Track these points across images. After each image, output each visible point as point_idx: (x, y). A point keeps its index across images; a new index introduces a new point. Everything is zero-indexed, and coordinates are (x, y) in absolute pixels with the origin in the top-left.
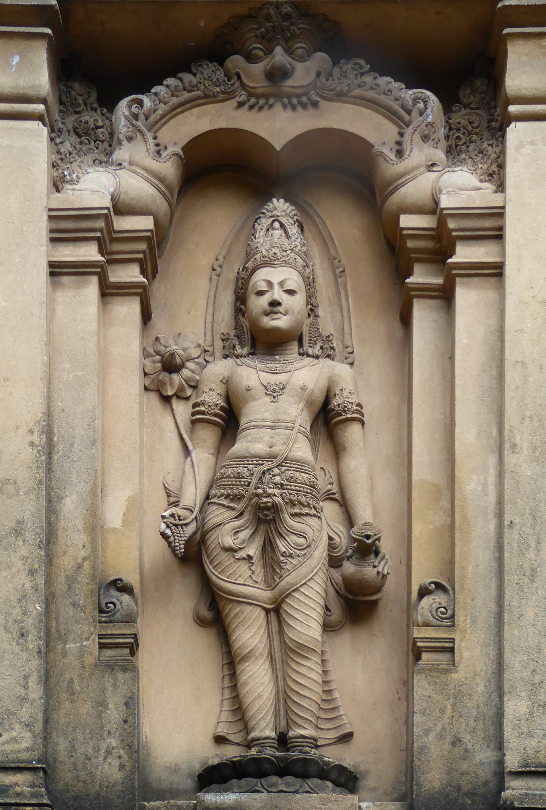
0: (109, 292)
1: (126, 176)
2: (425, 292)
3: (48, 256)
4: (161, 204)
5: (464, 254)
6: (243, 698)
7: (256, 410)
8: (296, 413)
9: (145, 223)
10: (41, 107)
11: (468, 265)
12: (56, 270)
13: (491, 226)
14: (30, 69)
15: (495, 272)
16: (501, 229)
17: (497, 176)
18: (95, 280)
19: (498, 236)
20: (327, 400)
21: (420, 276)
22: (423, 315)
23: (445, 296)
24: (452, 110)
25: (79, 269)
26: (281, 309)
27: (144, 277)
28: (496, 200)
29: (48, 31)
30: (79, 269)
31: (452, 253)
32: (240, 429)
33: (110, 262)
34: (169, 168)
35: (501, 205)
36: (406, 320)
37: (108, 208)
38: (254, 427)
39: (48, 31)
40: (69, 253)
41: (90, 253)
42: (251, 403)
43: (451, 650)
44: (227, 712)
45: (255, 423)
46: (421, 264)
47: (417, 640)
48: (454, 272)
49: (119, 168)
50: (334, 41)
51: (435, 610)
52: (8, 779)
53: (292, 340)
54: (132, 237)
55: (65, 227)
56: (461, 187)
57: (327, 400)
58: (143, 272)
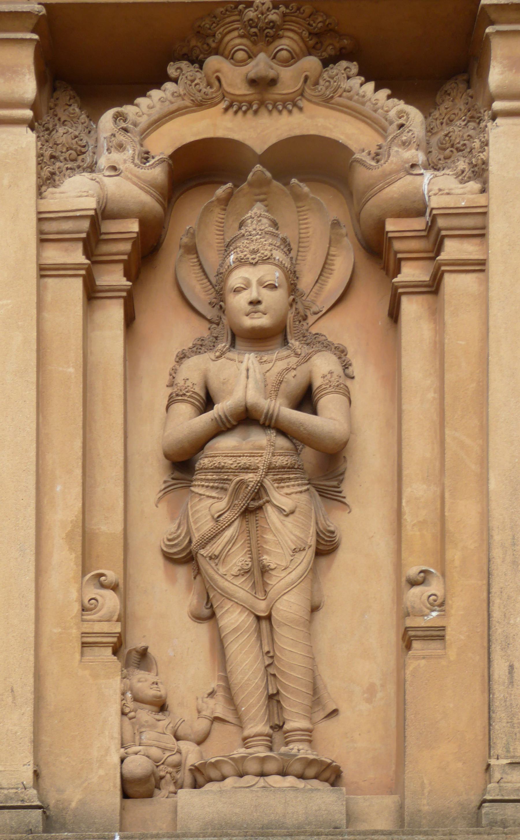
2: (416, 289)
5: (452, 249)
6: (224, 637)
15: (480, 266)
16: (484, 228)
19: (480, 234)
21: (411, 273)
22: (411, 308)
23: (434, 287)
24: (141, 224)
28: (481, 200)
33: (94, 263)
34: (157, 173)
36: (394, 314)
40: (54, 255)
42: (256, 634)
44: (207, 720)
46: (398, 257)
47: (412, 638)
48: (443, 268)
49: (113, 173)
50: (333, 45)
51: (426, 601)
56: (443, 189)
58: (127, 275)
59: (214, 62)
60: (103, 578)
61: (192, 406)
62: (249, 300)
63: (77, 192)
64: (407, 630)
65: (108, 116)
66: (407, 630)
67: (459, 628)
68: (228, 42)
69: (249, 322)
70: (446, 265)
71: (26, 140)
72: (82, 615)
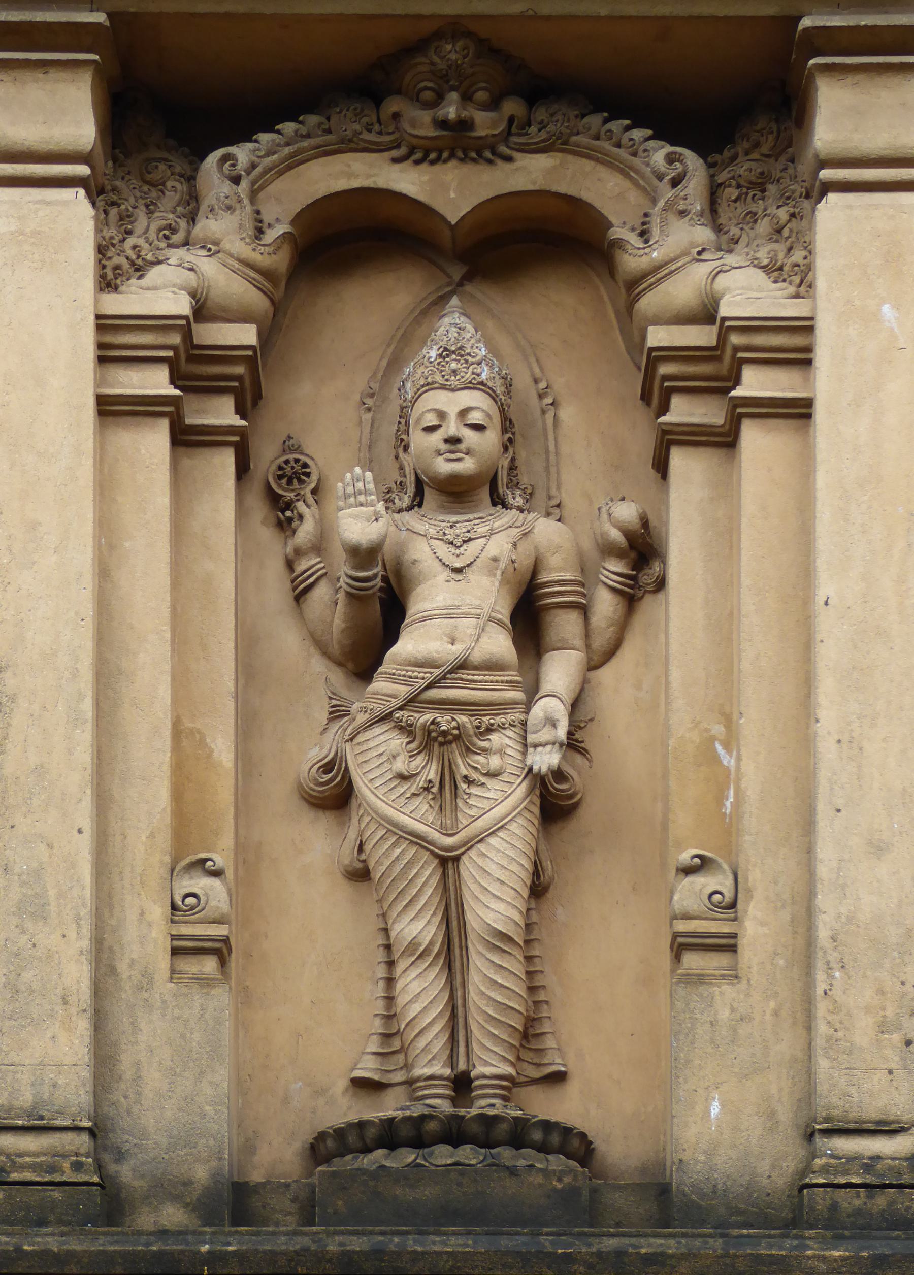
0: (185, 438)
1: (210, 261)
3: (97, 385)
4: (256, 299)
5: (755, 383)
7: (431, 596)
8: (488, 595)
9: (245, 335)
10: (83, 170)
11: (139, 399)
12: (110, 409)
13: (794, 345)
14: (64, 112)
16: (809, 349)
17: (803, 280)
18: (165, 424)
19: (803, 360)
20: (535, 573)
23: (725, 440)
25: (140, 408)
26: (462, 446)
27: (241, 419)
29: (97, 57)
30: (140, 408)
31: (737, 382)
32: (405, 622)
35: (810, 316)
37: (186, 317)
38: (427, 763)
39: (97, 57)
41: (156, 382)
43: (732, 949)
45: (425, 614)
52: (8, 1141)
53: (480, 486)
54: (223, 355)
55: (114, 342)
56: (747, 293)
57: (535, 573)
58: (241, 411)
59: (393, 105)
60: (209, 863)
61: (328, 813)
62: (446, 437)
63: (161, 294)
64: (676, 935)
65: (213, 158)
66: (676, 935)
67: (758, 928)
68: (420, 64)
69: (444, 467)
70: (743, 406)
71: (75, 212)
72: (172, 914)
